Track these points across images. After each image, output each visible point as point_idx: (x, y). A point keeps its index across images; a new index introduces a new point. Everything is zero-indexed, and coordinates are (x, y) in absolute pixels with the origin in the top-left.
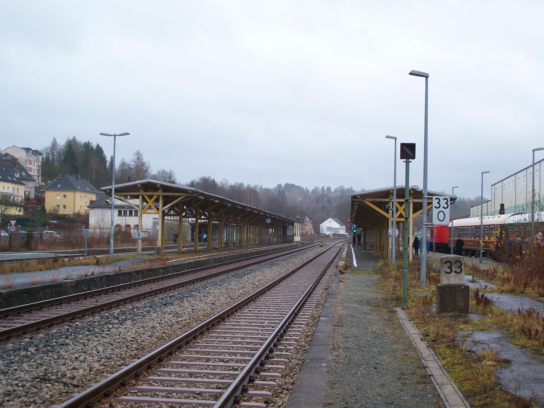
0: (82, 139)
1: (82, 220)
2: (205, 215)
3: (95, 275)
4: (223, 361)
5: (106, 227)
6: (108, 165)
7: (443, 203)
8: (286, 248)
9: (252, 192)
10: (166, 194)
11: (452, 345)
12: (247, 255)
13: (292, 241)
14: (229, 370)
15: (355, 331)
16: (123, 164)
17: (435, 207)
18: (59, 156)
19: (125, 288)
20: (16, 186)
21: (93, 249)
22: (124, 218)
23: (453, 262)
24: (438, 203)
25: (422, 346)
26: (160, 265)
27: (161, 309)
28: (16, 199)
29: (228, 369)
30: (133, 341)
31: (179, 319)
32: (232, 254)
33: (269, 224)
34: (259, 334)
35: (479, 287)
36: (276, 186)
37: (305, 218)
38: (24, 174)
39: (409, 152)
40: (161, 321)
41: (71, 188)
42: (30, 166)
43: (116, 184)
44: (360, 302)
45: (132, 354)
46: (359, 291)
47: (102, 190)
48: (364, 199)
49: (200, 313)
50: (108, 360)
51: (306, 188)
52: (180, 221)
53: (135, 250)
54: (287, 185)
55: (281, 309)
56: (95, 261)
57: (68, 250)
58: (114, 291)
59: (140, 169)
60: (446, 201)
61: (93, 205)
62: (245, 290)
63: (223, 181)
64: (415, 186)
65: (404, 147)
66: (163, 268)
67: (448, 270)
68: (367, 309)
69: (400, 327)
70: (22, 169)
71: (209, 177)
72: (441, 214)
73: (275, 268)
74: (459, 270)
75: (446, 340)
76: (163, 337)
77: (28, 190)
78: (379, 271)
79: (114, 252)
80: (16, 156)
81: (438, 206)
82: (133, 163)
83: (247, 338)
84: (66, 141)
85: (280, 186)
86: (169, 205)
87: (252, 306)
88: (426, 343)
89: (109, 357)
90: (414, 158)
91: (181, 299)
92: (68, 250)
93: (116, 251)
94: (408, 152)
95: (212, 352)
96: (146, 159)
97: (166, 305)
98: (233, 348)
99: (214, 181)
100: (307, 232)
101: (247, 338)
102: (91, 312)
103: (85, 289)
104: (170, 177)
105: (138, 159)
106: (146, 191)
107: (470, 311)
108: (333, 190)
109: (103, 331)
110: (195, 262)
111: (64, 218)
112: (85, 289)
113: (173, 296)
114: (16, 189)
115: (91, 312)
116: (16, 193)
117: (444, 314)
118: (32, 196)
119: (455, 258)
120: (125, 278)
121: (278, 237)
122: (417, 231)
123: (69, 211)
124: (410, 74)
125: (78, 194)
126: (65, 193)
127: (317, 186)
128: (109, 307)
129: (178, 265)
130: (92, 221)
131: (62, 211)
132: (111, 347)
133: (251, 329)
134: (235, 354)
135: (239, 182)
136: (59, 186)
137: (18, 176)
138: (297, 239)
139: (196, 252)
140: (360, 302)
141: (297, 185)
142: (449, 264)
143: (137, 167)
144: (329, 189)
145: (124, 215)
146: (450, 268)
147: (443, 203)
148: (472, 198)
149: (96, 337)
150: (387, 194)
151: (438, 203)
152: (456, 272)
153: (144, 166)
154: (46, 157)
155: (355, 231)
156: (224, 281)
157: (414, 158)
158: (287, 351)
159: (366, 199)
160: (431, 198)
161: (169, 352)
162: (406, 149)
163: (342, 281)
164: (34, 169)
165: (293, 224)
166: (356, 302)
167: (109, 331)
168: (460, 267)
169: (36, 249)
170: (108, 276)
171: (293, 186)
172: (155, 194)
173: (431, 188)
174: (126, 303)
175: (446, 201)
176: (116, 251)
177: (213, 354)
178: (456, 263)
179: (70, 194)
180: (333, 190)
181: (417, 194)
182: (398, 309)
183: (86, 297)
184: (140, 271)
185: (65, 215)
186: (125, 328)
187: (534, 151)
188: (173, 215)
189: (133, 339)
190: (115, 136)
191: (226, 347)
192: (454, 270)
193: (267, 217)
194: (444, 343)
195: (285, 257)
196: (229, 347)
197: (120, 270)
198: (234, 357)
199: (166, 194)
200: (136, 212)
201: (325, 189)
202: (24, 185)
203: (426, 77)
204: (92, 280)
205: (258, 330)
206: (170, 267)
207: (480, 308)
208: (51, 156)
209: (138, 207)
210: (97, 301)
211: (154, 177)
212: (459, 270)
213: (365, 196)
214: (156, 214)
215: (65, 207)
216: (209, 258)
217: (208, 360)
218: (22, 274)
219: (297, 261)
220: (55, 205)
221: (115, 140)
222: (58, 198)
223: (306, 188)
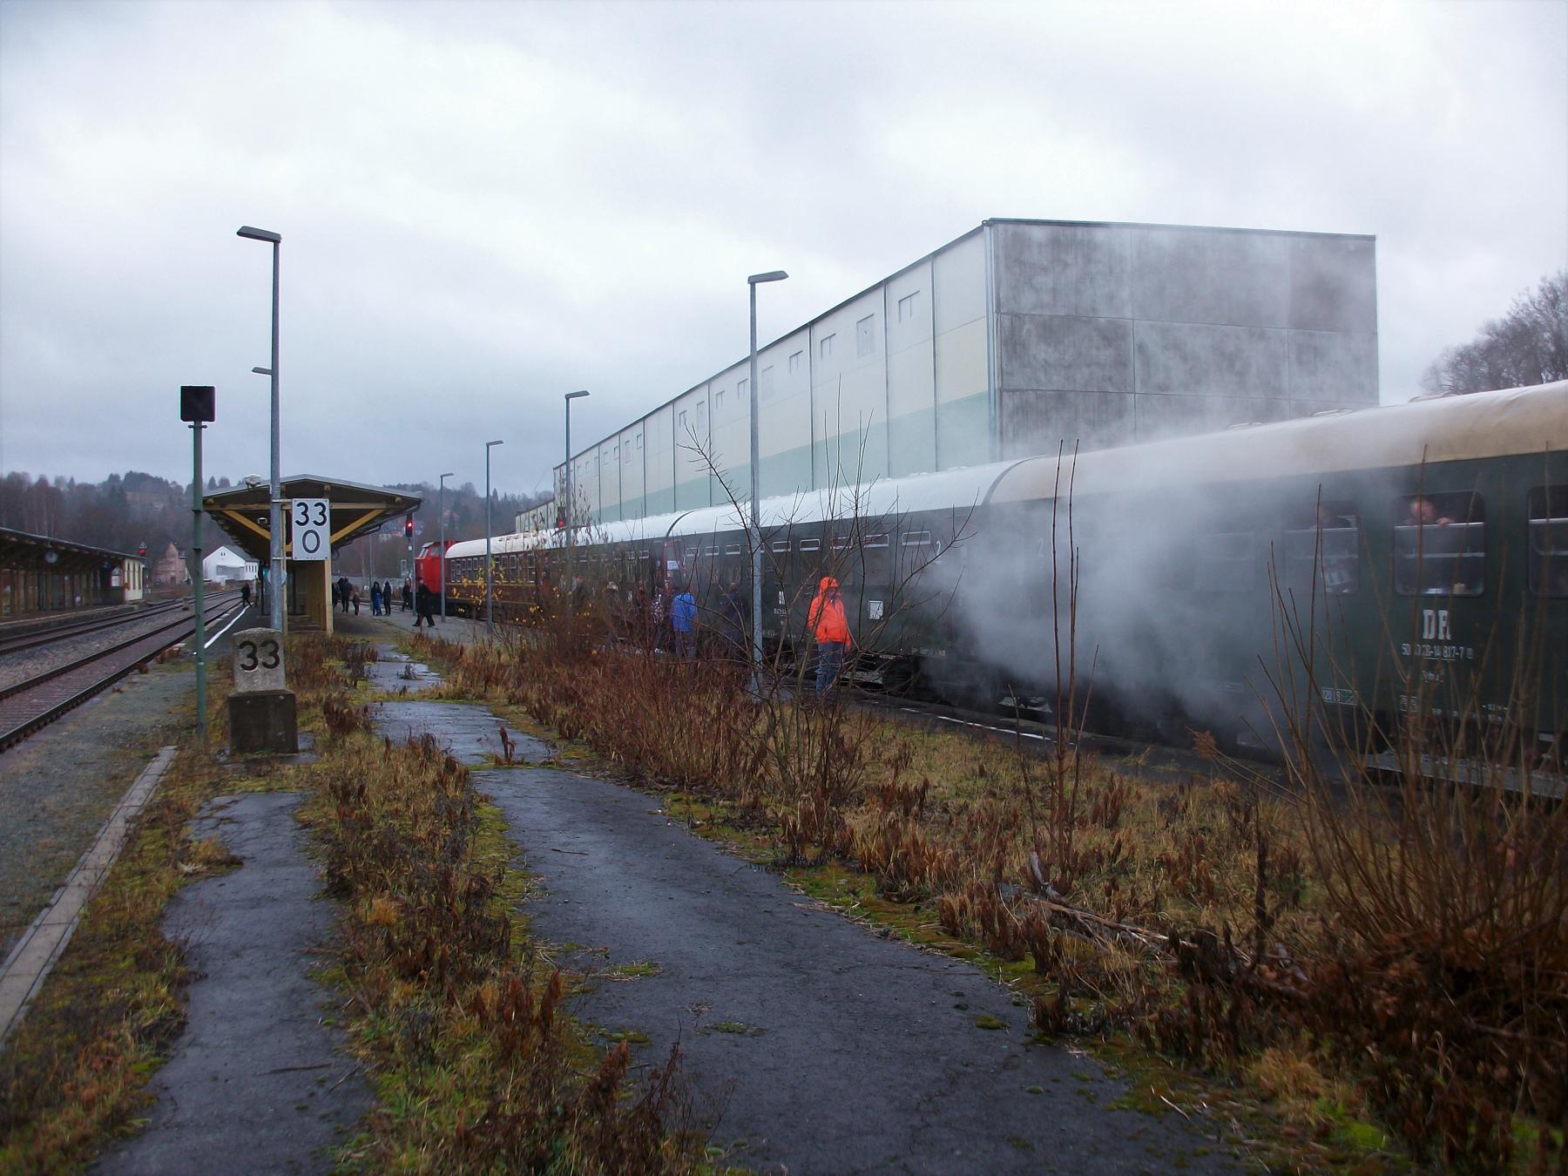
13: (121, 600)
24: (304, 513)
36: (106, 478)
37: (167, 548)
48: (223, 506)
54: (131, 476)
74: (273, 660)
90: (212, 419)
119: (261, 635)
124: (239, 233)
138: (134, 594)
141: (153, 474)
142: (248, 650)
146: (252, 656)
148: (530, 495)
151: (304, 513)
152: (265, 665)
157: (212, 419)
168: (274, 654)
171: (144, 477)
178: (264, 645)
192: (260, 660)
193: (48, 550)
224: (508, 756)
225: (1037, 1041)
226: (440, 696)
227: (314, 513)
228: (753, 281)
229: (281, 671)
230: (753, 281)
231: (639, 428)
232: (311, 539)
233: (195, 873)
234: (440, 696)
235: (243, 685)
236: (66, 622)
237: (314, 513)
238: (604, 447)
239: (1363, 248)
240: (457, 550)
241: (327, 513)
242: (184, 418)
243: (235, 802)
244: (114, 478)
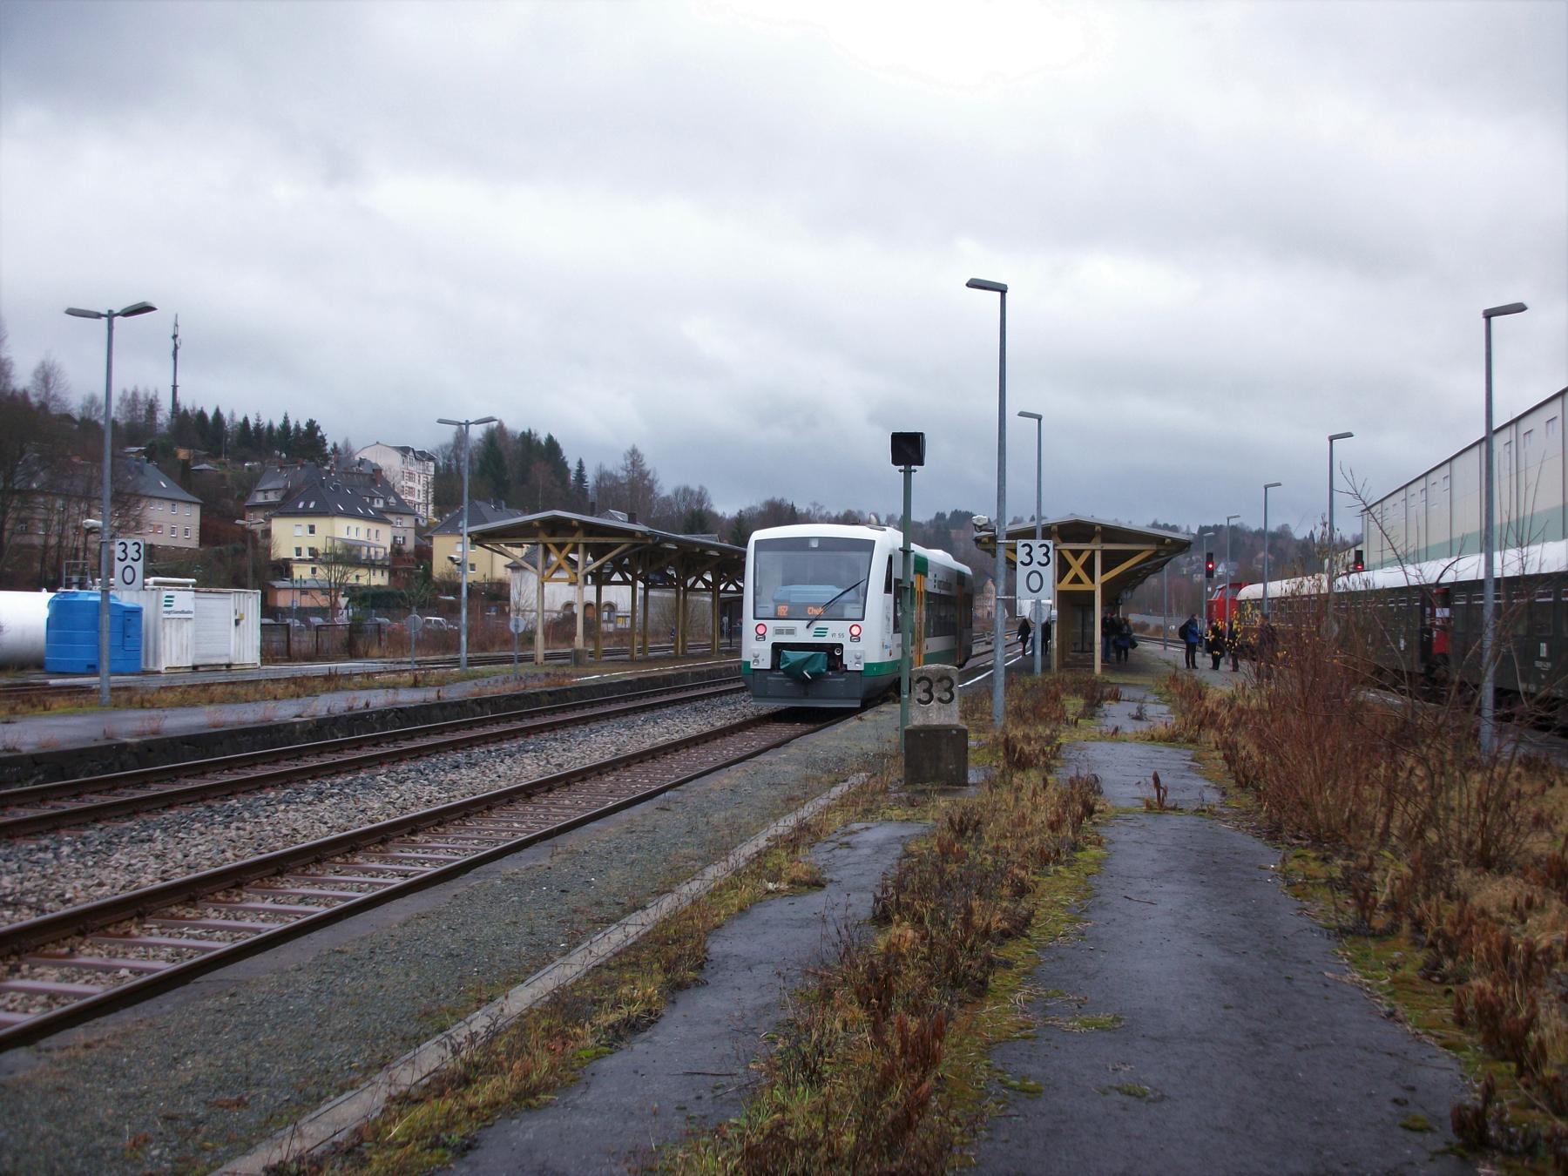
1: (497, 594)
10: (592, 540)
20: (374, 527)
24: (1029, 554)
28: (372, 551)
36: (932, 517)
38: (392, 500)
39: (909, 451)
42: (410, 484)
53: (531, 659)
66: (550, 693)
67: (925, 697)
70: (388, 489)
72: (1035, 577)
77: (401, 533)
80: (382, 462)
81: (1027, 560)
94: (908, 449)
96: (649, 464)
99: (793, 508)
105: (633, 464)
114: (373, 533)
116: (373, 540)
118: (410, 545)
119: (938, 671)
137: (380, 504)
142: (925, 684)
146: (928, 691)
151: (1029, 554)
152: (940, 700)
164: (416, 487)
168: (949, 690)
169: (366, 655)
170: (401, 710)
172: (570, 540)
184: (489, 700)
187: (1331, 439)
199: (592, 540)
202: (390, 523)
203: (1002, 290)
212: (947, 696)
215: (473, 567)
218: (233, 706)
224: (1161, 800)
225: (1452, 1151)
226: (1153, 738)
227: (1038, 554)
228: (1489, 315)
229: (955, 706)
230: (1489, 315)
231: (1445, 470)
232: (1035, 580)
233: (778, 891)
234: (1153, 738)
237: (1038, 554)
238: (1412, 489)
243: (867, 828)
244: (940, 516)
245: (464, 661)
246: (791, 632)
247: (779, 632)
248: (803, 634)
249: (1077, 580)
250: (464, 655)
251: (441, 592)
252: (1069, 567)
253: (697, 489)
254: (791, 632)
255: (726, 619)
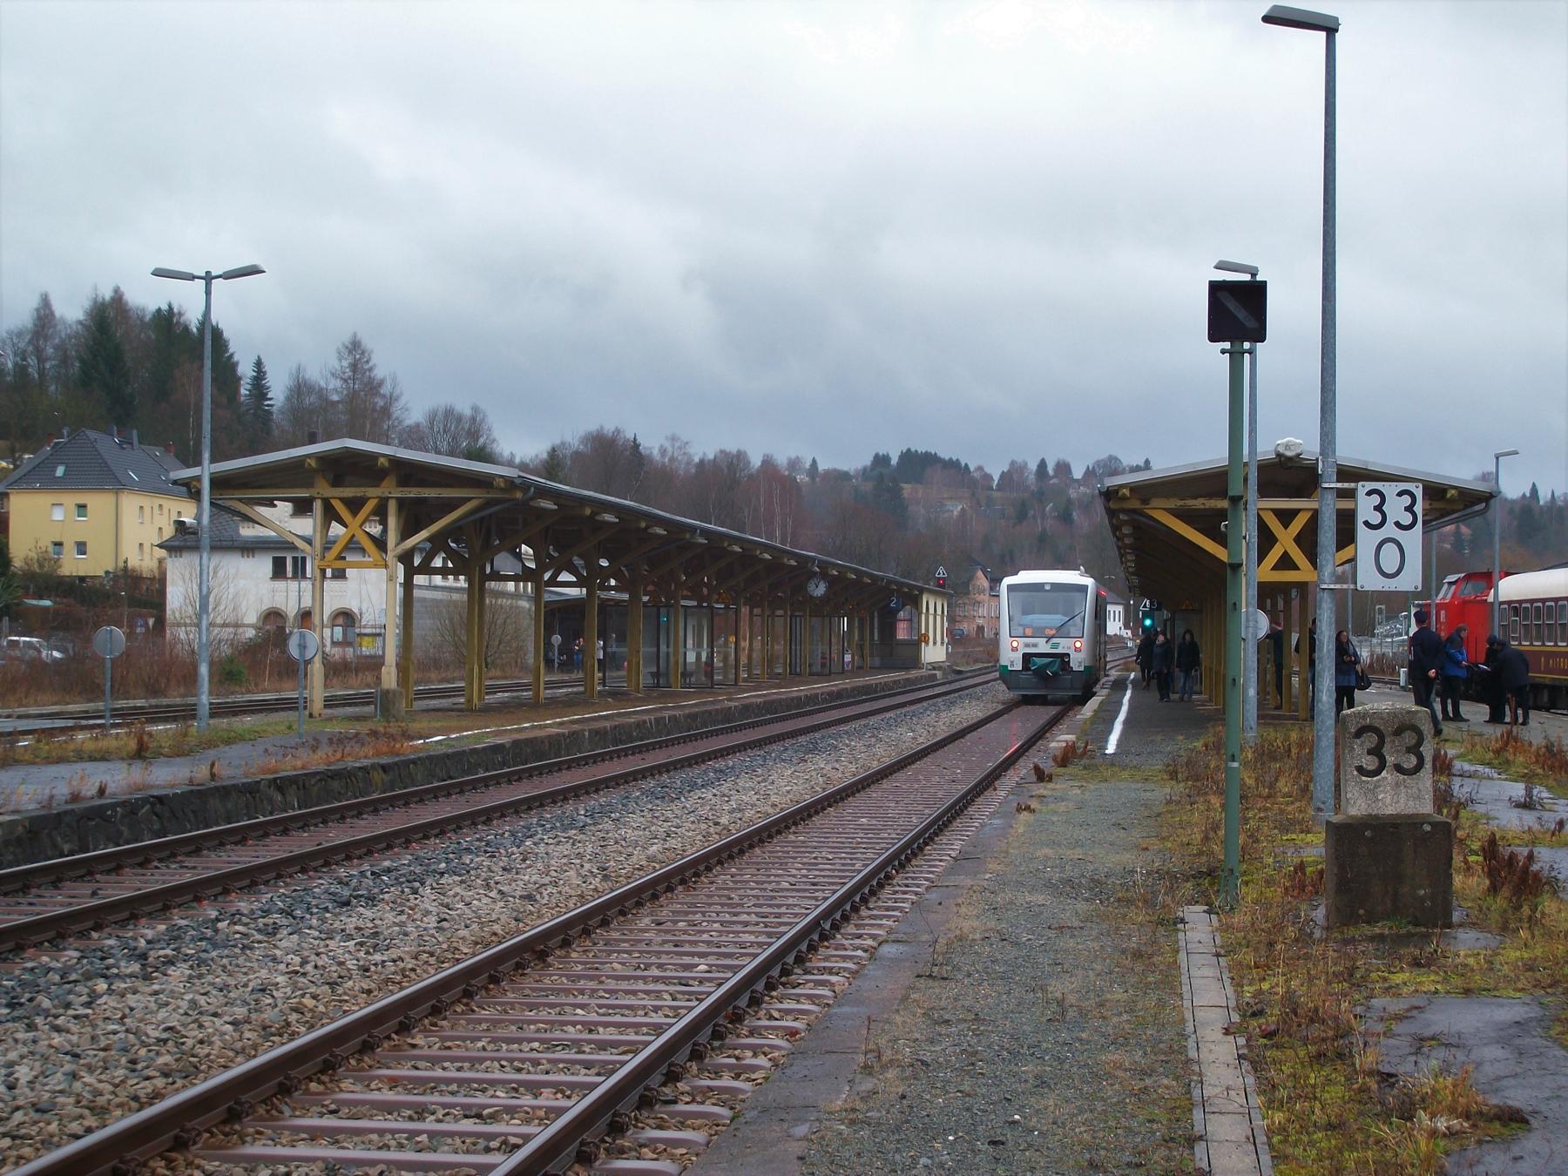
0: (147, 297)
1: (139, 595)
2: (572, 570)
3: (113, 795)
4: (479, 1116)
5: (219, 621)
6: (243, 391)
7: (1396, 508)
8: (886, 686)
9: (776, 480)
10: (413, 493)
11: (1334, 1050)
12: (727, 715)
13: (915, 662)
14: (488, 1150)
15: (986, 997)
16: (300, 388)
17: (1366, 523)
18: (64, 361)
19: (222, 844)
21: (165, 701)
22: (293, 585)
23: (1387, 730)
24: (1379, 508)
25: (1219, 1060)
26: (378, 754)
27: (324, 920)
29: (482, 1143)
30: (165, 1041)
31: (378, 957)
32: (666, 714)
33: (824, 600)
34: (656, 1009)
35: (1536, 827)
36: (867, 460)
37: (971, 578)
39: (1241, 314)
40: (304, 962)
41: (110, 480)
43: (213, 460)
44: (1067, 887)
45: (142, 1094)
46: (1077, 844)
47: (175, 482)
48: (1145, 501)
49: (464, 933)
50: (37, 1116)
51: (980, 468)
52: (477, 592)
55: (778, 916)
56: (133, 745)
57: (71, 708)
58: (174, 855)
59: (363, 401)
60: (1407, 500)
61: (183, 540)
62: (672, 843)
63: (667, 445)
64: (1287, 446)
65: (1222, 295)
66: (385, 768)
67: (1370, 763)
68: (1073, 910)
69: (1170, 980)
71: (618, 431)
72: (1390, 548)
73: (820, 762)
74: (1414, 760)
75: (1316, 1031)
76: (288, 1024)
78: (1193, 775)
79: (212, 715)
81: (1376, 518)
82: (335, 384)
83: (606, 1025)
84: (87, 304)
85: (881, 460)
86: (424, 534)
87: (668, 908)
88: (1242, 1041)
89: (43, 1106)
91: (415, 882)
92: (71, 708)
93: (217, 711)
94: (1237, 310)
95: (448, 1081)
96: (383, 365)
97: (347, 903)
98: (536, 1063)
99: (636, 446)
100: (980, 629)
101: (606, 1025)
102: (52, 934)
103: (66, 848)
104: (474, 434)
105: (354, 367)
106: (337, 482)
107: (1456, 916)
108: (1078, 474)
109: (68, 1006)
110: (516, 743)
111: (78, 590)
112: (66, 848)
113: (389, 870)
115: (52, 934)
117: (1352, 932)
120: (229, 805)
121: (861, 647)
122: (1388, 619)
123: (94, 565)
124: (1267, 19)
125: (131, 503)
126: (161, 502)
127: (1019, 459)
128: (126, 914)
129: (447, 756)
130: (177, 597)
131: (72, 565)
132: (68, 1067)
133: (634, 993)
134: (535, 1088)
135: (732, 448)
136: (60, 471)
138: (934, 653)
139: (536, 707)
140: (1067, 887)
141: (945, 455)
142: (1370, 740)
143: (352, 396)
144: (1063, 468)
145: (295, 577)
146: (1376, 752)
147: (1396, 508)
149: (31, 1027)
150: (1212, 482)
151: (1379, 508)
152: (1399, 769)
153: (377, 394)
154: (16, 364)
155: (1148, 622)
156: (605, 811)
158: (737, 1077)
159: (1155, 503)
160: (1351, 494)
161: (281, 1084)
162: (1232, 305)
163: (1028, 808)
165: (915, 601)
166: (1049, 885)
167: (88, 1005)
168: (1415, 749)
171: (929, 459)
172: (372, 492)
173: (1349, 452)
174: (198, 899)
175: (1407, 500)
176: (217, 711)
177: (454, 1087)
179: (99, 503)
180: (1078, 474)
181: (1289, 476)
182: (1195, 914)
183: (60, 880)
184: (293, 780)
185: (82, 579)
186: (156, 993)
188: (444, 572)
189: (165, 1035)
190: (208, 278)
191: (511, 1061)
192: (1390, 760)
194: (1305, 1041)
195: (873, 720)
196: (523, 1061)
197: (213, 776)
198: (527, 1100)
199: (413, 493)
200: (299, 565)
201: (1051, 471)
203: (1330, 28)
204: (97, 813)
205: (658, 995)
206: (414, 762)
207: (1500, 902)
208: (32, 361)
209: (309, 541)
210: (94, 894)
211: (414, 437)
213: (1149, 491)
214: (376, 566)
215: (81, 547)
216: (576, 727)
217: (421, 1112)
219: (909, 734)
220: (46, 543)
221: (208, 293)
222: (58, 515)
223: (980, 468)
232: (1390, 552)
235: (1357, 805)
236: (839, 695)
239: (355, 335)
240: (1515, 587)
241: (1418, 508)
242: (1213, 338)
244: (881, 460)
245: (204, 710)
246: (1035, 645)
247: (1027, 645)
248: (1043, 647)
249: (1286, 563)
250: (205, 699)
251: (27, 596)
252: (1298, 540)
253: (468, 412)
254: (1035, 645)
255: (557, 639)
